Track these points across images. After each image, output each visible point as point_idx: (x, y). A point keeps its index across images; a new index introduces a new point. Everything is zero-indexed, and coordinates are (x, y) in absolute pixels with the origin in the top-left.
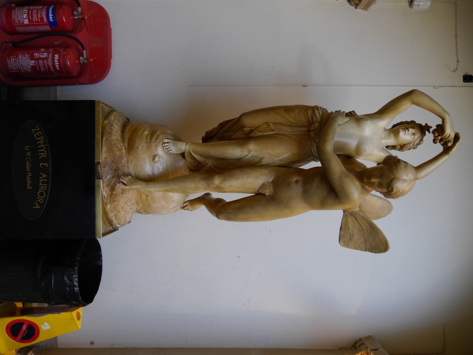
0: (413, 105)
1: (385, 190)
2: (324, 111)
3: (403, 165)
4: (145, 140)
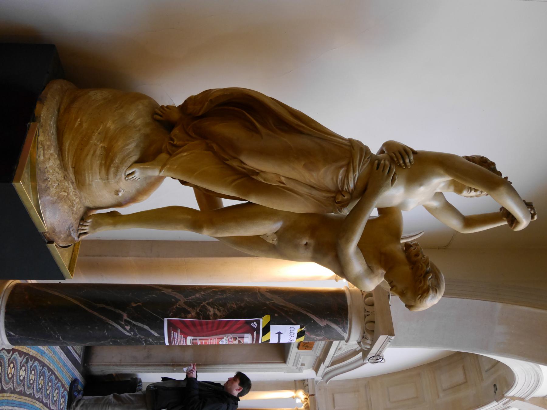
4: (98, 174)
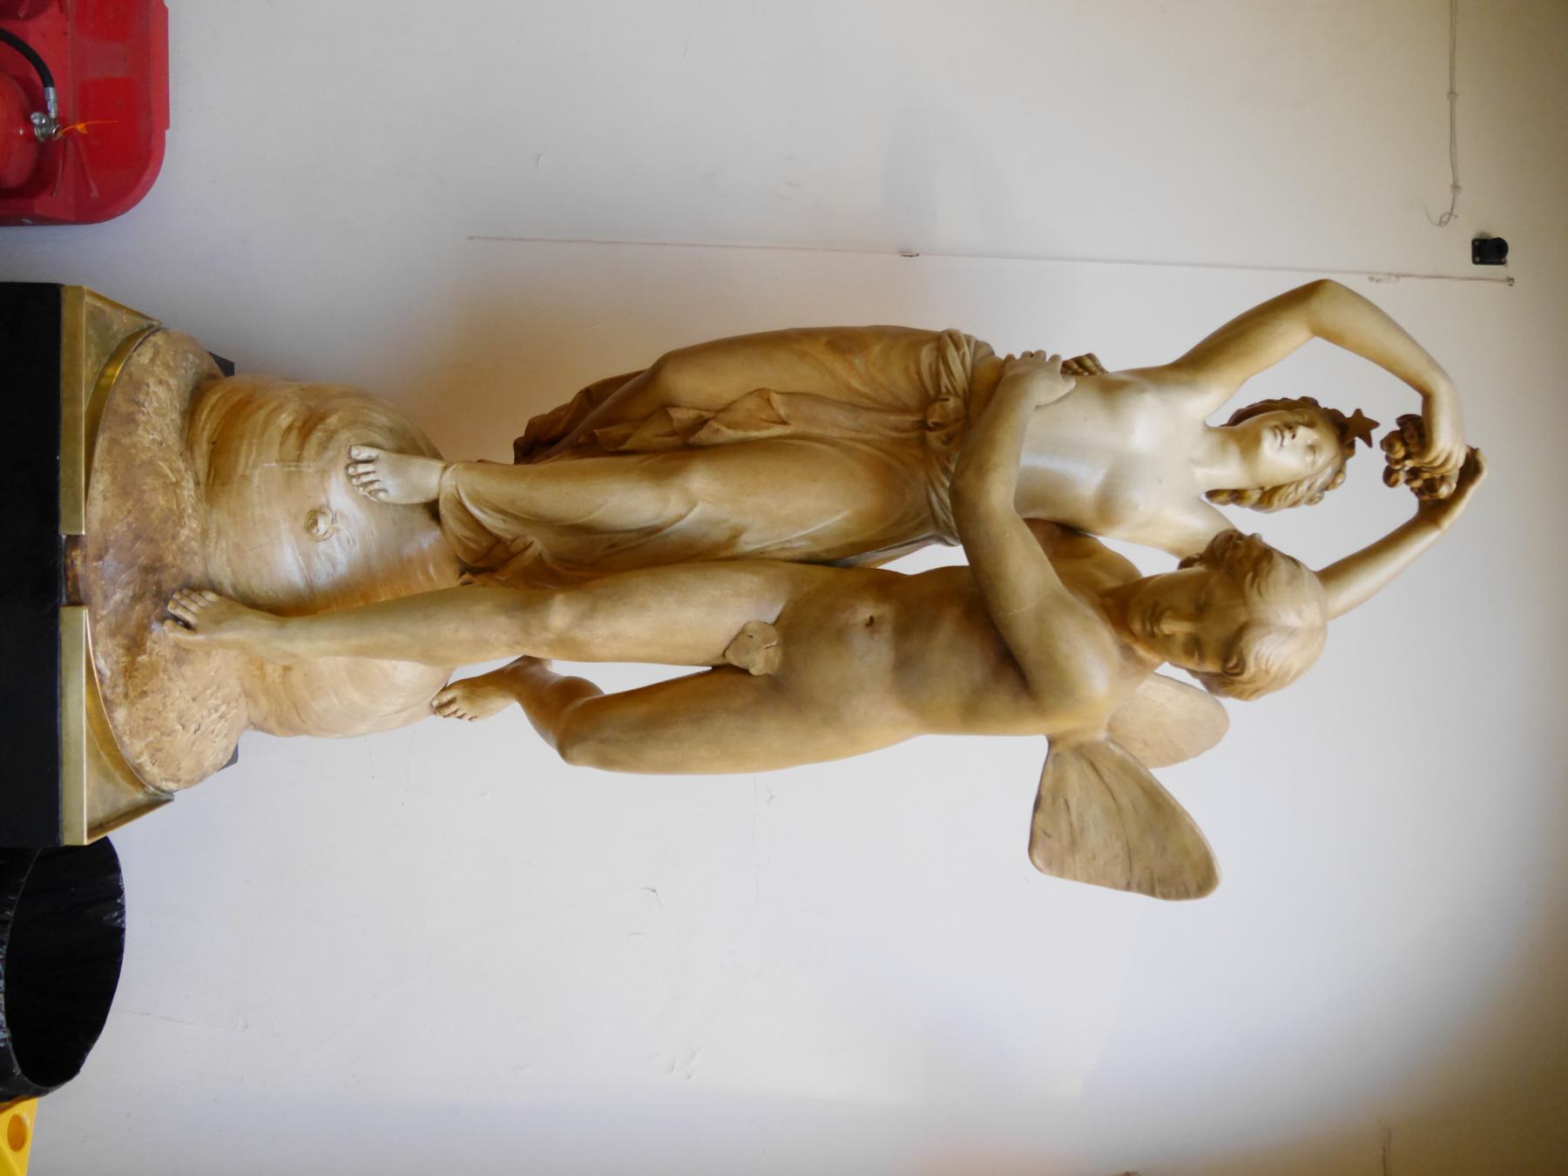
0: (1318, 340)
1: (1211, 667)
2: (980, 354)
3: (1282, 571)
4: (276, 447)
